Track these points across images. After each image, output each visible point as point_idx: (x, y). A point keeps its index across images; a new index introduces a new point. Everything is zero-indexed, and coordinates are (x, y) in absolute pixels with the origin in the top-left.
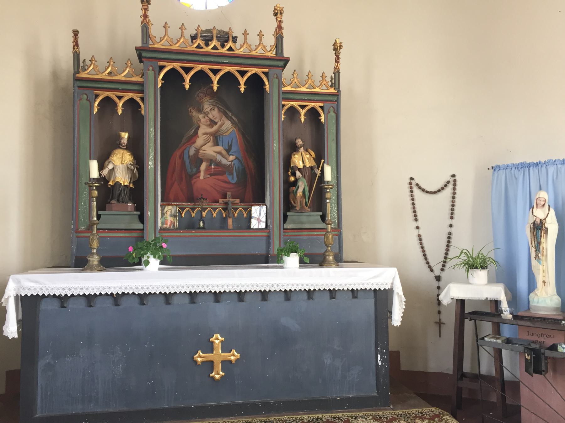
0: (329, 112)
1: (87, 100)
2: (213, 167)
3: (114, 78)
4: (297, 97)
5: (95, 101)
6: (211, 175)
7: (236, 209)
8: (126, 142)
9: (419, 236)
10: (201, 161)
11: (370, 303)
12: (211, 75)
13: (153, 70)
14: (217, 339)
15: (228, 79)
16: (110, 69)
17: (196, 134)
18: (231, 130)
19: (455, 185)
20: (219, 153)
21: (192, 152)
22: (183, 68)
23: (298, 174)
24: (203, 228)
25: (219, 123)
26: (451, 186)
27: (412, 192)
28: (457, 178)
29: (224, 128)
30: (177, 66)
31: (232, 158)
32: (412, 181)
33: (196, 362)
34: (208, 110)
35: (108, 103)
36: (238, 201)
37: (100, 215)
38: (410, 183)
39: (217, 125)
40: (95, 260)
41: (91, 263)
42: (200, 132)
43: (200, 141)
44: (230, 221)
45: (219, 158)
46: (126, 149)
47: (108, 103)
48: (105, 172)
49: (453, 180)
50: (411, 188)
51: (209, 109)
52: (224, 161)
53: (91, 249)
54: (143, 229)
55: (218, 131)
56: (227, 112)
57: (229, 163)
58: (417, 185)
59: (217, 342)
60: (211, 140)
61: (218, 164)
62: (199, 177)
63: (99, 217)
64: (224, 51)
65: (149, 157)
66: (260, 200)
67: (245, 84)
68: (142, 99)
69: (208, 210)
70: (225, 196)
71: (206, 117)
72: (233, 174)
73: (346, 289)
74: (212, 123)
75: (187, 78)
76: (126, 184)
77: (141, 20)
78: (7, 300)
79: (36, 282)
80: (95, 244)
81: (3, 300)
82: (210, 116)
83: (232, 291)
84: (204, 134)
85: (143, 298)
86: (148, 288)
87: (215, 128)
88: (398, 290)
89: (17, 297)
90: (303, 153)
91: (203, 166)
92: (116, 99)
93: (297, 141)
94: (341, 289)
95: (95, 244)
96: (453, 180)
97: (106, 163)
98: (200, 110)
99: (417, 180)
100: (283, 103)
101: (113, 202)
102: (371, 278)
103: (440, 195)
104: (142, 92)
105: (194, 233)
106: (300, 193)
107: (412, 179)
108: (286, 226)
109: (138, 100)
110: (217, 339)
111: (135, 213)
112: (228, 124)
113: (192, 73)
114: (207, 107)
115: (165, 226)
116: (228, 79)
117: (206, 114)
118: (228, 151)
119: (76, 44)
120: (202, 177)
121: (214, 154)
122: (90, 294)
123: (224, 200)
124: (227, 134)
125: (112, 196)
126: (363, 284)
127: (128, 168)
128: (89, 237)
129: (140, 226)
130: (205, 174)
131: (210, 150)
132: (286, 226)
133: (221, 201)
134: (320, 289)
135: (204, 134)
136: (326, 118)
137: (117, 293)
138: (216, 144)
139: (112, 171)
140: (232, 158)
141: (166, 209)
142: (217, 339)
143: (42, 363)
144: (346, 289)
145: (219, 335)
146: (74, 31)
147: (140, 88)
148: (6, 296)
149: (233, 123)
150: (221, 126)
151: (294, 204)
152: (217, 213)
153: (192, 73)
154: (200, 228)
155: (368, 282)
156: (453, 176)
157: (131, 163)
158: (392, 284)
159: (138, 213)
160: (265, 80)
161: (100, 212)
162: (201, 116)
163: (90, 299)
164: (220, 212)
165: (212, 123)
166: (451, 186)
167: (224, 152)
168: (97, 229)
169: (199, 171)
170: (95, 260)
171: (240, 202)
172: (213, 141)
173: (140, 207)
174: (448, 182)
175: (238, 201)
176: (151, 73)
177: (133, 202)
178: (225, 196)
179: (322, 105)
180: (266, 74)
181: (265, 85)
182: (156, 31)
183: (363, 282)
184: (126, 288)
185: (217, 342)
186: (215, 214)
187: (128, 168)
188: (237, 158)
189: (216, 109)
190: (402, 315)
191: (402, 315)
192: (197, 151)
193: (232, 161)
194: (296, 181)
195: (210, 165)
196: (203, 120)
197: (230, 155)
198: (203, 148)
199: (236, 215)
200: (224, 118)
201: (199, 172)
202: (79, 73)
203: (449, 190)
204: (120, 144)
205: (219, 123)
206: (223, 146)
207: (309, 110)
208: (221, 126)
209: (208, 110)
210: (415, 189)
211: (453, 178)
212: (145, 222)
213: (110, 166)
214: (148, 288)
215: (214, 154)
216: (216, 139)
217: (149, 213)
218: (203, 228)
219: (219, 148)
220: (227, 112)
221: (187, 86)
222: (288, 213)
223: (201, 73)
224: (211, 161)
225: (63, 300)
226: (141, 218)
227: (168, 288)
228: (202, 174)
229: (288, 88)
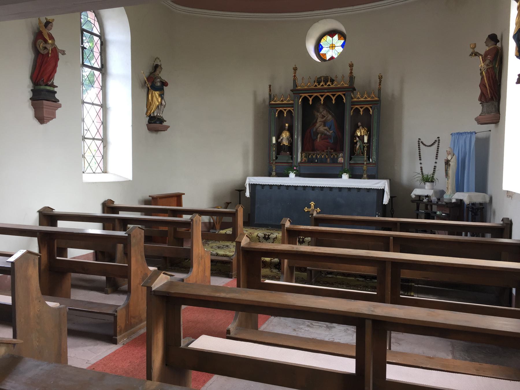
0: (374, 109)
1: (274, 112)
2: (323, 136)
3: (283, 102)
4: (358, 103)
5: (276, 112)
6: (322, 139)
7: (332, 154)
8: (287, 128)
9: (421, 167)
10: (318, 134)
11: (375, 194)
12: (320, 97)
13: (297, 98)
14: (312, 203)
15: (328, 98)
16: (282, 99)
17: (316, 122)
18: (331, 119)
19: (439, 142)
20: (326, 130)
21: (314, 130)
22: (309, 96)
23: (357, 139)
24: (317, 162)
25: (326, 117)
26: (437, 143)
27: (419, 145)
28: (440, 139)
29: (329, 118)
30: (306, 95)
31: (331, 132)
32: (420, 140)
33: (305, 211)
34: (322, 111)
35: (281, 112)
36: (332, 151)
37: (278, 157)
38: (419, 141)
39: (326, 117)
40: (274, 173)
41: (273, 174)
42: (318, 121)
43: (318, 125)
44: (328, 160)
45: (326, 132)
46: (288, 130)
47: (281, 112)
48: (280, 140)
49: (438, 141)
50: (419, 143)
51: (322, 110)
52: (328, 133)
53: (273, 170)
54: (292, 163)
55: (325, 120)
56: (330, 111)
57: (330, 134)
58: (422, 142)
59: (312, 205)
60: (323, 124)
61: (325, 135)
62: (317, 140)
63: (277, 158)
64: (325, 86)
65: (295, 133)
66: (342, 150)
67: (335, 100)
68: (293, 110)
69: (311, 155)
70: (327, 149)
71: (321, 114)
72: (331, 139)
73: (363, 188)
74: (323, 116)
75: (311, 99)
76: (287, 145)
77: (293, 78)
78: (246, 184)
79: (254, 179)
80: (274, 168)
81: (245, 185)
82: (323, 114)
83: (318, 186)
84: (319, 122)
85: (288, 187)
86: (297, 184)
87: (324, 119)
88: (387, 190)
89: (249, 184)
90: (361, 129)
91: (319, 136)
92: (284, 111)
93: (359, 124)
94: (361, 188)
95: (274, 168)
96: (438, 141)
97: (280, 136)
98: (318, 111)
99: (422, 140)
100: (352, 106)
101: (282, 152)
102: (374, 184)
103: (432, 147)
104: (293, 107)
105: (312, 164)
106: (358, 147)
107: (419, 139)
108: (350, 162)
109: (292, 110)
110: (312, 203)
111: (290, 156)
112: (330, 117)
113: (312, 97)
114: (321, 110)
115: (302, 161)
116: (328, 98)
117: (321, 113)
118: (330, 129)
119: (270, 90)
120: (318, 141)
121: (324, 130)
122: (270, 185)
123: (327, 150)
124: (329, 121)
125: (282, 150)
126: (371, 186)
127: (288, 138)
128: (272, 165)
129: (291, 161)
130: (320, 139)
131: (322, 129)
132: (350, 162)
133: (325, 151)
134: (364, 188)
135: (319, 122)
136: (373, 112)
137: (279, 185)
138: (325, 126)
139: (282, 140)
140: (331, 132)
141: (303, 154)
142: (312, 204)
143: (256, 206)
144: (363, 188)
145: (313, 202)
146: (269, 85)
147: (292, 105)
148: (246, 184)
149: (332, 116)
150: (327, 118)
151: (355, 153)
152: (324, 156)
153: (312, 97)
154: (316, 162)
155: (373, 185)
156: (438, 138)
157: (289, 136)
158: (385, 187)
159: (291, 156)
160: (344, 97)
161: (277, 156)
162: (318, 114)
163: (271, 186)
164: (325, 156)
165: (323, 116)
166: (437, 143)
167: (328, 129)
168: (275, 162)
169: (317, 138)
170: (274, 173)
171: (334, 151)
172: (323, 125)
173: (291, 154)
174: (436, 141)
175: (332, 151)
176: (296, 99)
177: (289, 152)
178: (327, 149)
179: (371, 106)
180: (344, 94)
181: (343, 100)
182: (299, 82)
183: (371, 185)
184: (290, 183)
185: (312, 205)
186: (314, 157)
187: (288, 138)
188: (333, 132)
189: (325, 111)
190: (389, 200)
191: (389, 200)
192: (317, 129)
193: (331, 133)
194: (357, 142)
195: (322, 135)
196: (319, 116)
197: (330, 131)
198: (319, 128)
199: (332, 157)
200: (328, 114)
201: (317, 138)
202: (271, 102)
203: (436, 145)
204: (285, 128)
205: (326, 117)
206: (327, 126)
207: (364, 109)
208: (327, 118)
209: (322, 111)
210: (421, 144)
211: (438, 139)
212: (293, 160)
213: (282, 138)
214: (288, 184)
215: (324, 130)
216: (325, 123)
217: (295, 156)
218: (317, 162)
219: (326, 128)
220: (330, 111)
221: (311, 103)
222: (352, 157)
223: (316, 97)
224: (322, 133)
225: (263, 186)
226: (292, 158)
227: (295, 184)
228: (318, 139)
229: (355, 100)
